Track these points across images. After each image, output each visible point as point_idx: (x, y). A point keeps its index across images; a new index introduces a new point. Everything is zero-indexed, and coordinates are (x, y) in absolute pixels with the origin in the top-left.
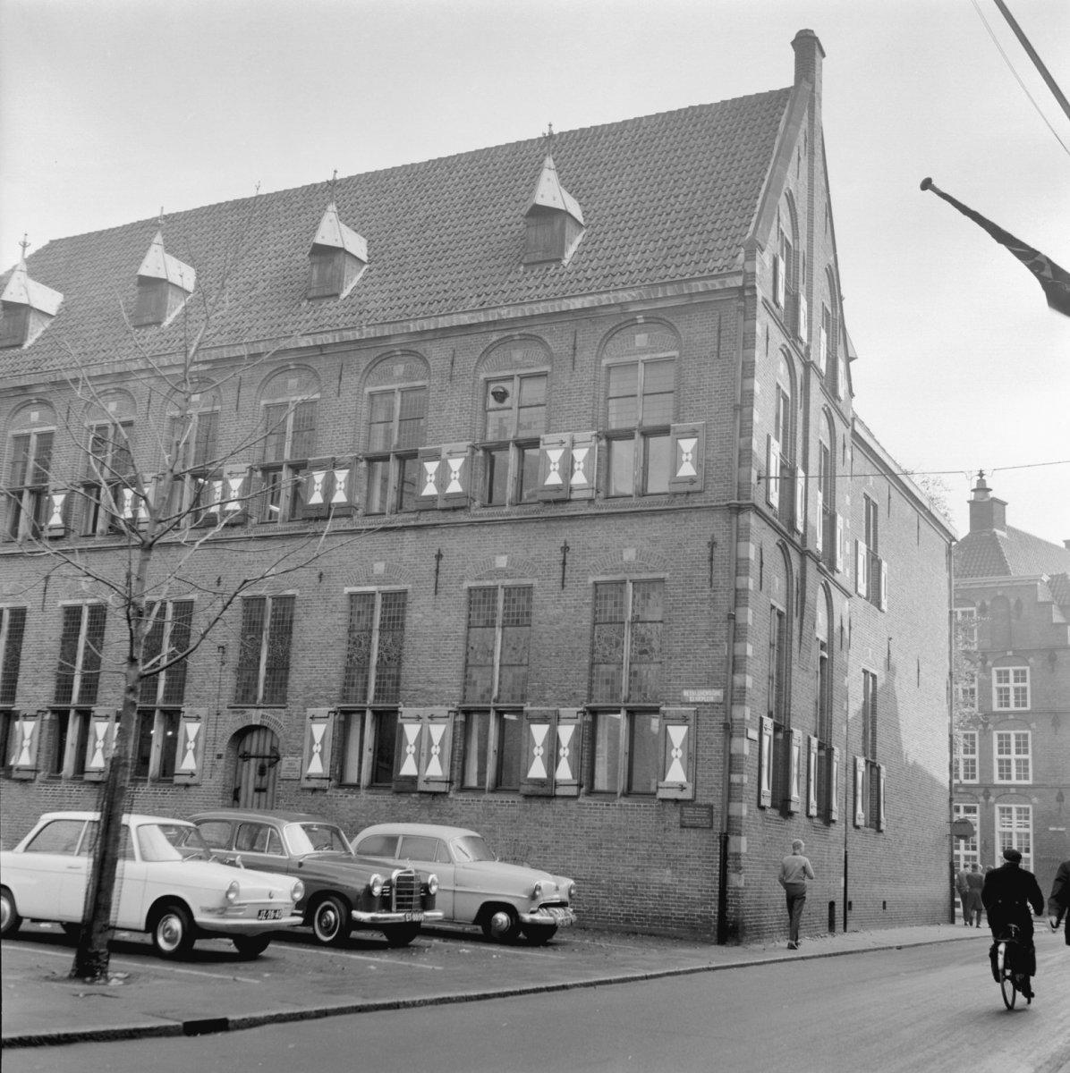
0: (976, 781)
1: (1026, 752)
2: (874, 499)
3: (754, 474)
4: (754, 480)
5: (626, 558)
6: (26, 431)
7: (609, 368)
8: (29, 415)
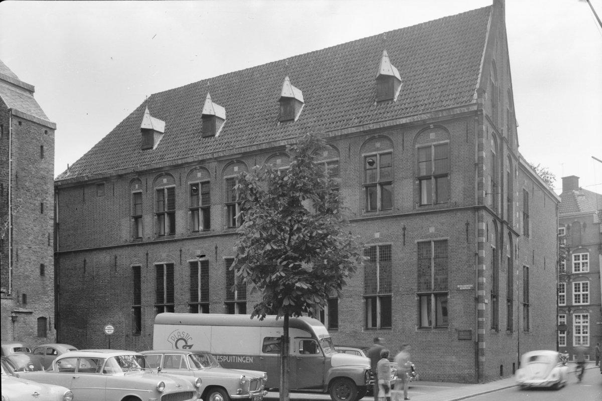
0: (565, 305)
1: (587, 290)
2: (527, 190)
3: (484, 192)
4: (484, 195)
5: (430, 231)
6: (162, 187)
7: (419, 148)
8: (163, 180)
